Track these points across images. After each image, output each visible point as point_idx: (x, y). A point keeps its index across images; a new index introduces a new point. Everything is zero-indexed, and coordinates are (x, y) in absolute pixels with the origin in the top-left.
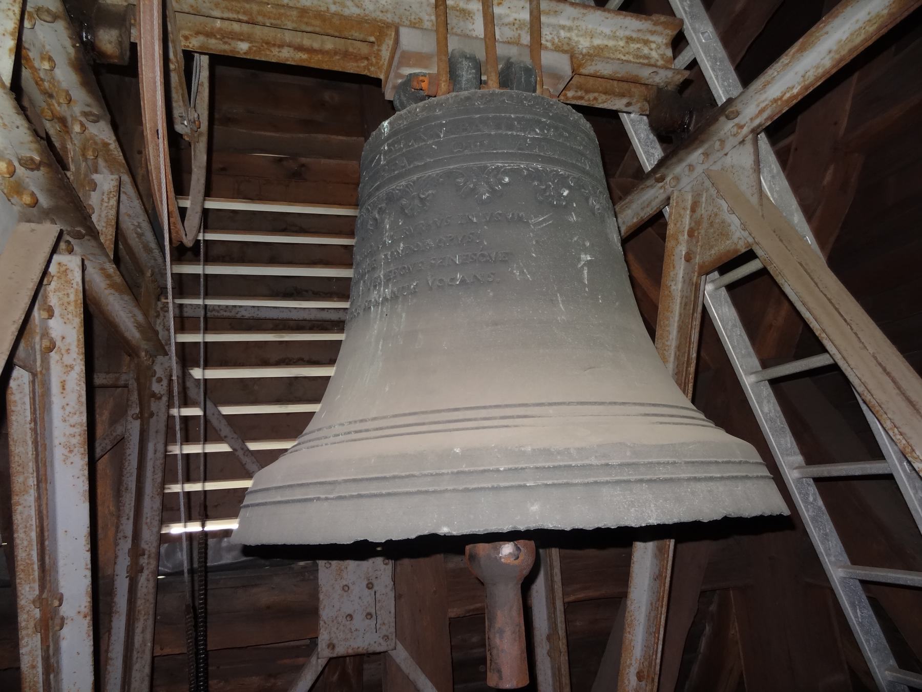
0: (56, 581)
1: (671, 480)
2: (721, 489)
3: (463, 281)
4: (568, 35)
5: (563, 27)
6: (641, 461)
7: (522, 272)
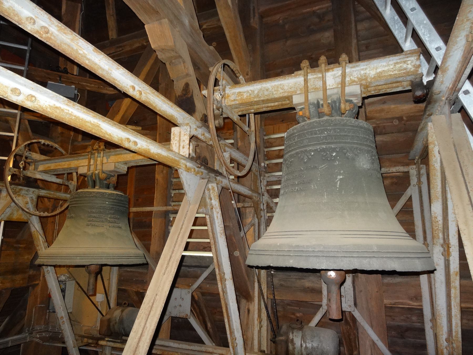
0: (223, 269)
1: (334, 256)
2: (356, 260)
3: (297, 190)
4: (365, 72)
5: (363, 69)
6: (325, 250)
7: (314, 186)
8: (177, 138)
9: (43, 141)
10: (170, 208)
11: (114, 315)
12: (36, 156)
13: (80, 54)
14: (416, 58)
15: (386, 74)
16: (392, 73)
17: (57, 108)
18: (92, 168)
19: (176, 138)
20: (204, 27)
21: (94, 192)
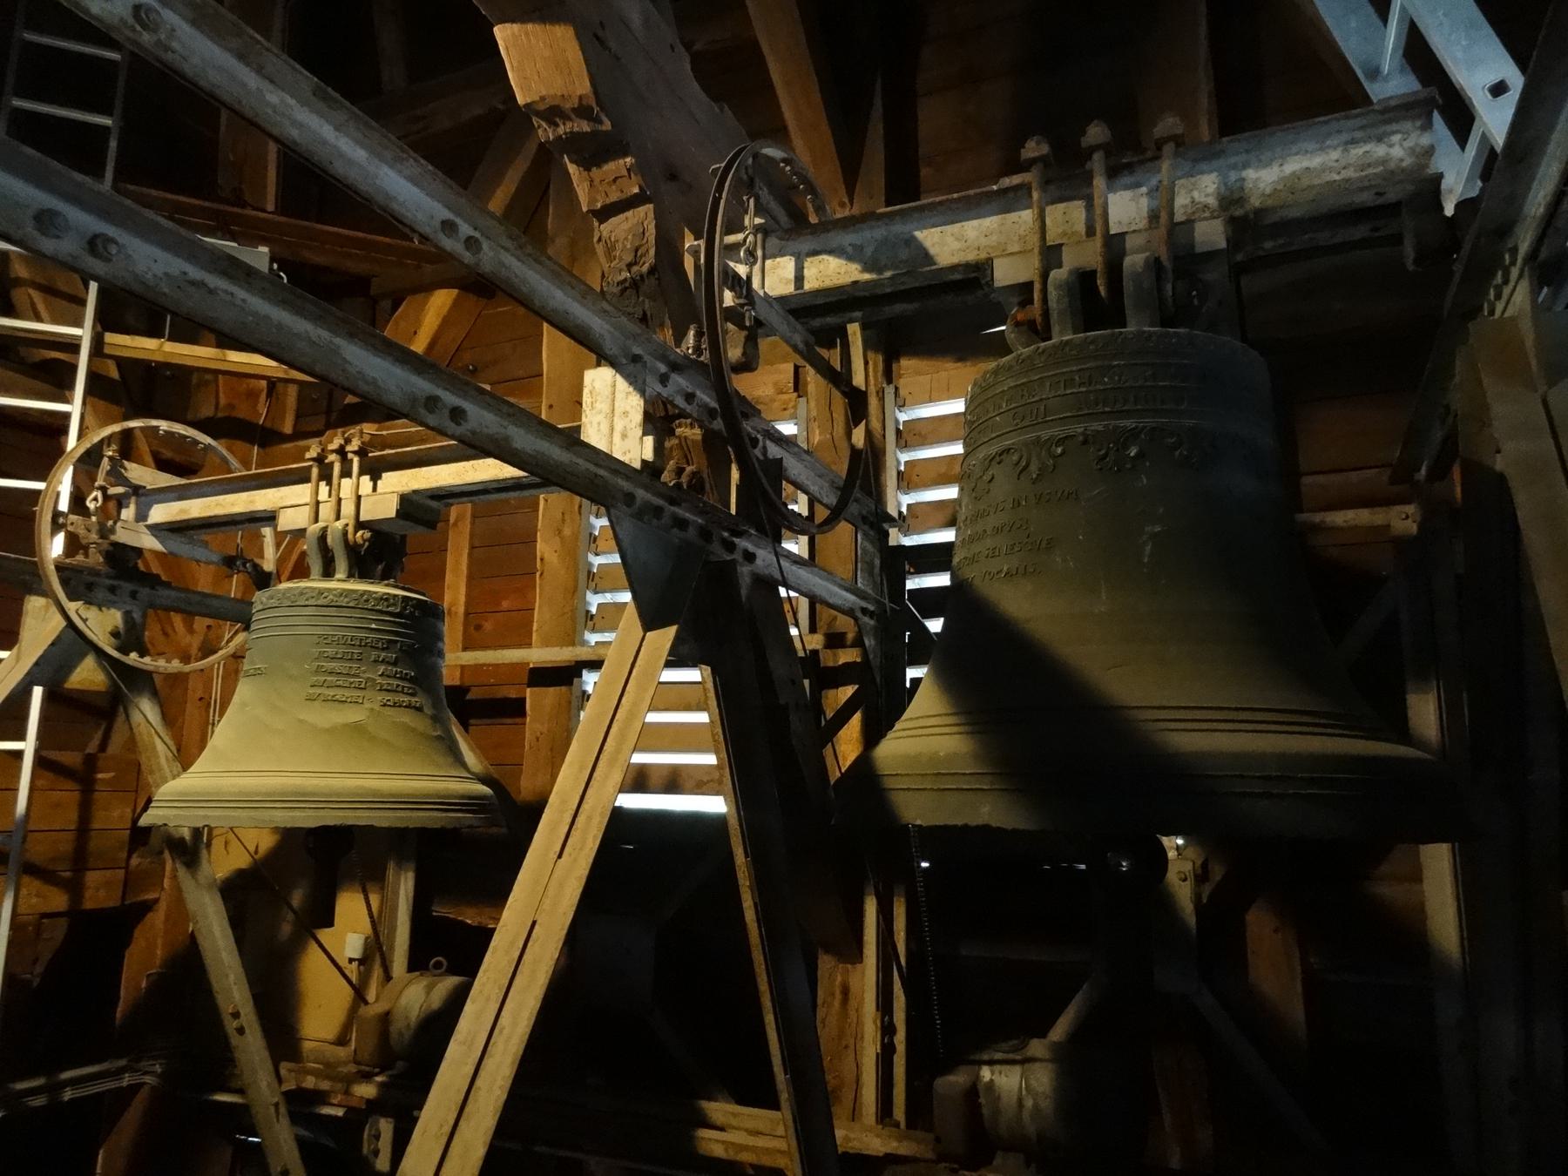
8: (603, 406)
9: (164, 425)
10: (581, 653)
11: (403, 1001)
12: (141, 474)
13: (268, 104)
14: (1418, 123)
15: (1316, 181)
16: (1337, 178)
17: (193, 283)
18: (326, 511)
19: (598, 406)
20: (697, 47)
21: (329, 590)
